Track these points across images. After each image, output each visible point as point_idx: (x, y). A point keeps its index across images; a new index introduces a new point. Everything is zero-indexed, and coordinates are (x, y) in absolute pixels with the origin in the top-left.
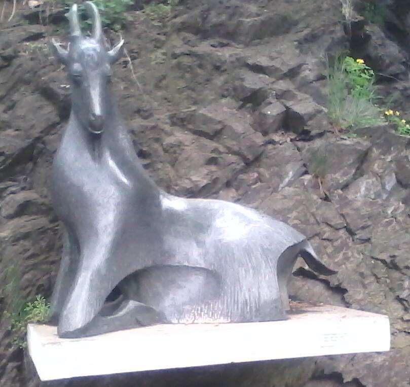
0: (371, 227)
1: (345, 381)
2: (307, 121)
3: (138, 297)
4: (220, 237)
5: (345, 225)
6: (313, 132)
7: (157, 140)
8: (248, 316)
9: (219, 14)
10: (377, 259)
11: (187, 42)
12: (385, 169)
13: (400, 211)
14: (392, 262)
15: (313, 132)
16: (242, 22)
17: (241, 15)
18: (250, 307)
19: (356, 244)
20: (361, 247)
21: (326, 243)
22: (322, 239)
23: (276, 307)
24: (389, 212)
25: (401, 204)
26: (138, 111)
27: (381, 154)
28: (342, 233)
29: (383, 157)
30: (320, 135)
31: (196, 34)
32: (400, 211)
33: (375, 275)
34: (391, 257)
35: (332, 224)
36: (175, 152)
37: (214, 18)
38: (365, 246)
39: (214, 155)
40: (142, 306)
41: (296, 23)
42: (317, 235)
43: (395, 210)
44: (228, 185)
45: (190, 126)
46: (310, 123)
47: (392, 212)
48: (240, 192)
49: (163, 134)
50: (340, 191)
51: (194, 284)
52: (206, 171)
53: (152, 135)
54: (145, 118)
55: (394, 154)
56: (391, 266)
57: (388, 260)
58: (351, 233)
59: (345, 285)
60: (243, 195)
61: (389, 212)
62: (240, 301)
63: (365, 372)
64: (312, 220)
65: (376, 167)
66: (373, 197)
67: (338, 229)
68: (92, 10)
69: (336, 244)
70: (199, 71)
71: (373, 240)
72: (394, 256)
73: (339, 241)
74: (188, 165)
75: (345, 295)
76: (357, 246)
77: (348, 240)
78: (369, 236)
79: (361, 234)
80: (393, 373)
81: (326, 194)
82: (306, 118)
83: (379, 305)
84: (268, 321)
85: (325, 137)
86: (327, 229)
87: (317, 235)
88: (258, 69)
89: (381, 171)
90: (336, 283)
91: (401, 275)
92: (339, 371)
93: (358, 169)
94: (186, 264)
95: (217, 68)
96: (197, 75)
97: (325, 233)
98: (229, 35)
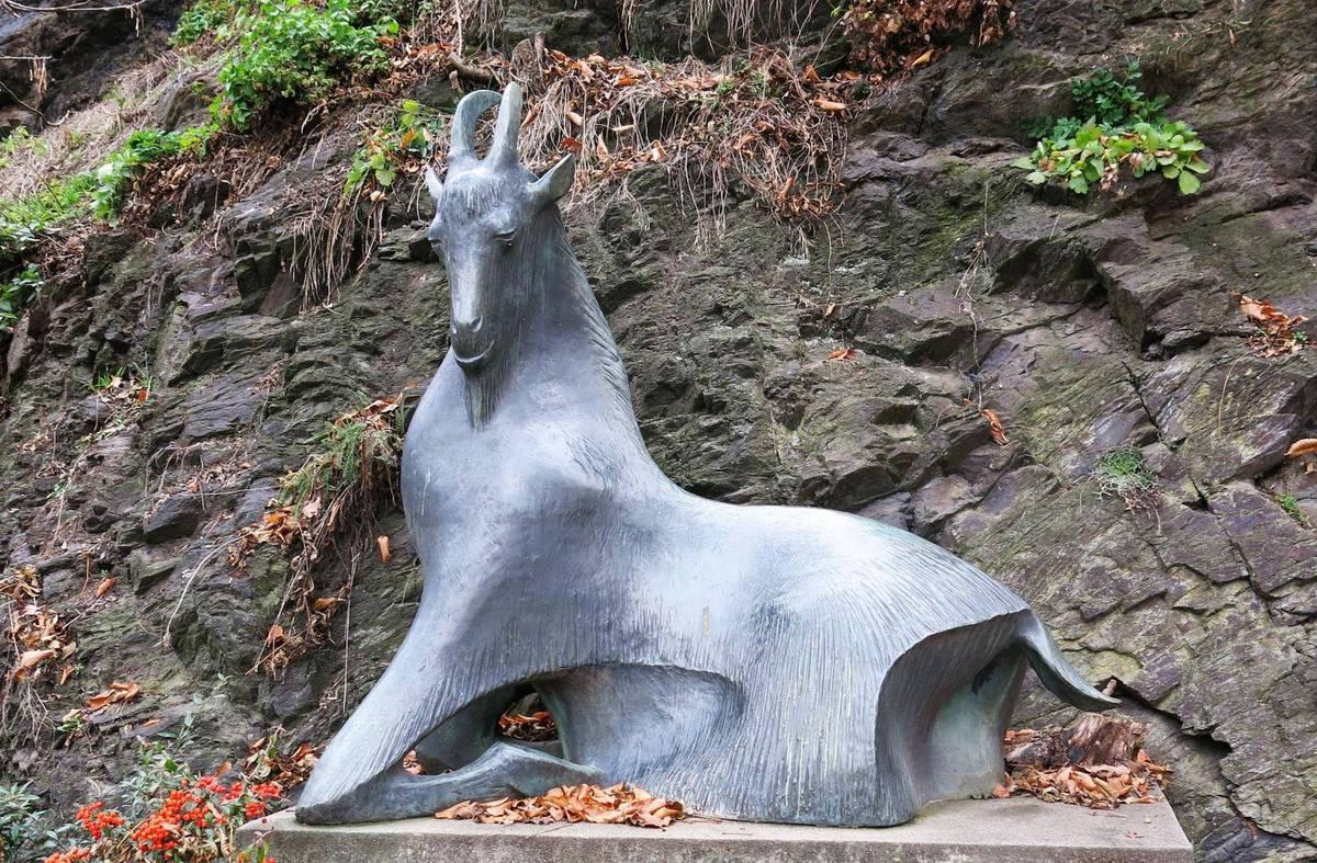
3: (545, 736)
4: (780, 600)
5: (1245, 573)
7: (747, 373)
8: (784, 808)
11: (885, 150)
18: (794, 785)
19: (1279, 624)
22: (1174, 608)
26: (718, 310)
30: (1197, 343)
31: (917, 133)
38: (1308, 631)
39: (906, 401)
40: (533, 763)
48: (977, 488)
49: (768, 357)
50: (1246, 487)
51: (692, 710)
52: (869, 438)
58: (1266, 598)
59: (1223, 733)
62: (771, 767)
67: (1220, 585)
68: (466, 103)
70: (906, 212)
74: (829, 425)
75: (1222, 762)
76: (1282, 630)
77: (1253, 615)
81: (1200, 494)
84: (834, 826)
85: (1212, 346)
86: (1188, 583)
87: (1162, 596)
90: (1200, 725)
94: (681, 663)
97: (1181, 593)
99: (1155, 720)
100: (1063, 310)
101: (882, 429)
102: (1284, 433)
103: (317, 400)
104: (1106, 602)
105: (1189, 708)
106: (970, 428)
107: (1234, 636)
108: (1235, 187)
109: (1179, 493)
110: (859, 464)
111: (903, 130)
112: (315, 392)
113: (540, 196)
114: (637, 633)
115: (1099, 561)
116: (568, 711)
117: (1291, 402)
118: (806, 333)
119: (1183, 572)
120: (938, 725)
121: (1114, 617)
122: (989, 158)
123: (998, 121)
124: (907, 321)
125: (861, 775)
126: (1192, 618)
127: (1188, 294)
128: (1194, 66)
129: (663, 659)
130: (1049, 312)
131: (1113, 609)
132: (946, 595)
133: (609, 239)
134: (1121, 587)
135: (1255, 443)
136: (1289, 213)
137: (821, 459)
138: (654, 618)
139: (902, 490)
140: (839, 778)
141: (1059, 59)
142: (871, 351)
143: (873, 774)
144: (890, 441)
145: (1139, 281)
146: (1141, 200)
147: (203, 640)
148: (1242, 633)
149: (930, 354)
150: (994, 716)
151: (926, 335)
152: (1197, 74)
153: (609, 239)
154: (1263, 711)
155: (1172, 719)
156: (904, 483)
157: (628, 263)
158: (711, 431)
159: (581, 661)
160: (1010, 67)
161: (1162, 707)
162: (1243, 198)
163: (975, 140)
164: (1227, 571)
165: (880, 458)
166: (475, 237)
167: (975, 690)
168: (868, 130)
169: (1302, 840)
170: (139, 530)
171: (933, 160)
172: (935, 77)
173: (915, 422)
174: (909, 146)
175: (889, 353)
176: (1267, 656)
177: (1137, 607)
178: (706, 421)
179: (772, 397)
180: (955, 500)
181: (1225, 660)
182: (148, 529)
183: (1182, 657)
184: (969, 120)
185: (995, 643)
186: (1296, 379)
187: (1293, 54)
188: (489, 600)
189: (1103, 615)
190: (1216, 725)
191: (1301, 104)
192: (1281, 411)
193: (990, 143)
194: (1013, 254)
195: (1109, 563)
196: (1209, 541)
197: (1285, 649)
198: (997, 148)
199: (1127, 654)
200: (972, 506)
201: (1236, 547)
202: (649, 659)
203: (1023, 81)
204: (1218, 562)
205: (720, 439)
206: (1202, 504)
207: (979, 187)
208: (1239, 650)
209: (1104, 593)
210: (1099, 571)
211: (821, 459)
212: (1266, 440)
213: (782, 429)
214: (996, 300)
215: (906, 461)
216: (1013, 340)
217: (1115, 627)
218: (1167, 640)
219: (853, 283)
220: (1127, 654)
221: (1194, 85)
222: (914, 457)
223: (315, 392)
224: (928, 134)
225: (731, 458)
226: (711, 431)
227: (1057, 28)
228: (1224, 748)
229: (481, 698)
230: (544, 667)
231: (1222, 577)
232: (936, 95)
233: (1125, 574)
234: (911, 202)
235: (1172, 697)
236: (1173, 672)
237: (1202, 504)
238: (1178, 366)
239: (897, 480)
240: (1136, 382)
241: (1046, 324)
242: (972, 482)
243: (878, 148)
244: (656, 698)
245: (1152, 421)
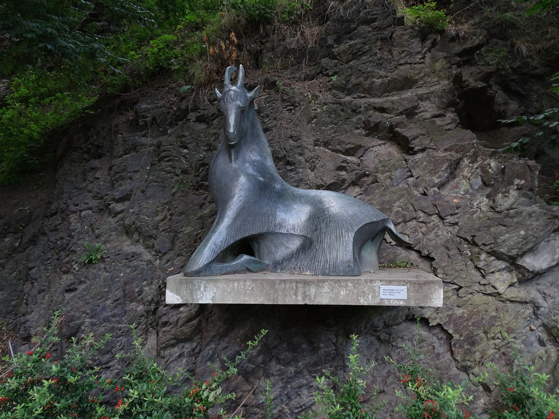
0: (459, 215)
1: (430, 325)
2: (412, 140)
6: (416, 149)
7: (301, 154)
8: (327, 271)
9: (358, 77)
10: (461, 238)
12: (472, 173)
13: (484, 204)
14: (472, 240)
15: (416, 149)
16: (373, 82)
17: (374, 77)
19: (445, 226)
20: (451, 229)
21: (421, 225)
23: (349, 266)
24: (475, 204)
25: (485, 199)
27: (470, 163)
28: (435, 218)
29: (471, 165)
30: (423, 150)
32: (484, 204)
33: (459, 249)
34: (472, 236)
35: (426, 211)
36: (313, 162)
37: (353, 80)
39: (344, 164)
40: (252, 260)
41: (416, 81)
42: (415, 218)
43: (480, 203)
44: (354, 184)
45: (330, 147)
46: (414, 142)
47: (477, 205)
48: (363, 189)
50: (436, 189)
53: (299, 151)
54: (296, 141)
55: (479, 163)
56: (471, 243)
57: (469, 239)
58: (442, 219)
59: (433, 255)
60: (364, 191)
61: (475, 204)
63: (447, 319)
64: (411, 208)
65: (465, 173)
66: (462, 193)
67: (431, 215)
69: (429, 225)
70: (341, 113)
71: (460, 224)
72: (475, 236)
73: (432, 223)
75: (433, 263)
77: (439, 223)
78: (457, 221)
79: (450, 219)
80: (470, 324)
82: (410, 139)
83: (460, 271)
86: (422, 214)
87: (415, 218)
88: (382, 110)
89: (470, 175)
90: (427, 253)
91: (479, 250)
92: (426, 317)
93: (452, 173)
95: (354, 111)
96: (340, 116)
97: (420, 217)
98: (369, 91)
99: (413, 252)
100: (384, 142)
101: (337, 172)
102: (446, 175)
103: (168, 161)
104: (400, 220)
105: (423, 248)
106: (361, 172)
107: (434, 229)
108: (426, 111)
109: (418, 191)
110: (333, 181)
111: (339, 90)
112: (167, 159)
113: (251, 97)
114: (279, 223)
115: (398, 209)
116: (259, 247)
117: (448, 166)
118: (316, 145)
119: (421, 212)
120: (363, 250)
121: (402, 224)
122: (363, 99)
123: (365, 89)
124: (344, 142)
125: (349, 261)
126: (423, 224)
127: (421, 137)
128: (417, 78)
129: (287, 231)
130: (380, 142)
131: (402, 222)
132: (367, 214)
133: (260, 116)
134: (404, 216)
135: (439, 177)
136: (440, 119)
137: (322, 179)
138: (284, 219)
139: (342, 189)
140: (342, 262)
141: (382, 73)
142: (333, 151)
143: (352, 261)
144: (340, 175)
145: (407, 133)
146: (404, 112)
147: (137, 230)
148: (436, 229)
149: (348, 152)
150: (376, 248)
151: (348, 146)
152: (417, 80)
153: (260, 116)
154: (443, 249)
155: (419, 252)
156: (342, 188)
157: (265, 123)
158: (291, 171)
159: (264, 231)
160: (369, 74)
161: (415, 248)
162: (429, 114)
163: (359, 94)
164: (432, 211)
165: (338, 180)
166: (234, 107)
167: (372, 241)
168: (330, 89)
169: (454, 283)
170: (114, 198)
171: (348, 98)
172: (349, 76)
173: (346, 170)
174: (341, 95)
175: (338, 151)
176: (442, 234)
177: (408, 221)
178: (289, 168)
179: (308, 162)
180: (357, 192)
181: (432, 236)
182: (117, 198)
183: (420, 235)
184: (358, 89)
185: (380, 227)
186: (451, 160)
187: (443, 75)
188: (239, 212)
189: (399, 223)
190: (158, 335)
191: (444, 89)
192: (446, 169)
193: (363, 95)
194: (372, 125)
195: (400, 209)
196: (426, 203)
197: (447, 233)
198: (364, 97)
199: (406, 234)
200: (361, 194)
201: (435, 205)
202: (284, 231)
203: (373, 78)
204: (431, 210)
205: (294, 173)
206: (425, 194)
207: (361, 107)
208: (436, 233)
209: (400, 217)
210: (398, 211)
211: (322, 179)
212: (442, 177)
213: (310, 171)
214: (366, 138)
215: (344, 181)
216: (372, 149)
217: (402, 227)
218: (416, 230)
219: (329, 132)
220: (406, 234)
221: (416, 83)
222: (346, 180)
223: (167, 159)
224: (345, 93)
225: (297, 179)
226: (291, 171)
227: (382, 64)
228: (433, 259)
229: (237, 241)
230: (254, 233)
231: (431, 213)
232: (349, 81)
233: (405, 212)
234: (342, 110)
235: (418, 245)
236: (419, 239)
237: (425, 194)
238: (419, 156)
239: (341, 186)
240: (406, 160)
241: (380, 145)
242: (361, 188)
243: (333, 95)
244: (285, 242)
245: (410, 172)
